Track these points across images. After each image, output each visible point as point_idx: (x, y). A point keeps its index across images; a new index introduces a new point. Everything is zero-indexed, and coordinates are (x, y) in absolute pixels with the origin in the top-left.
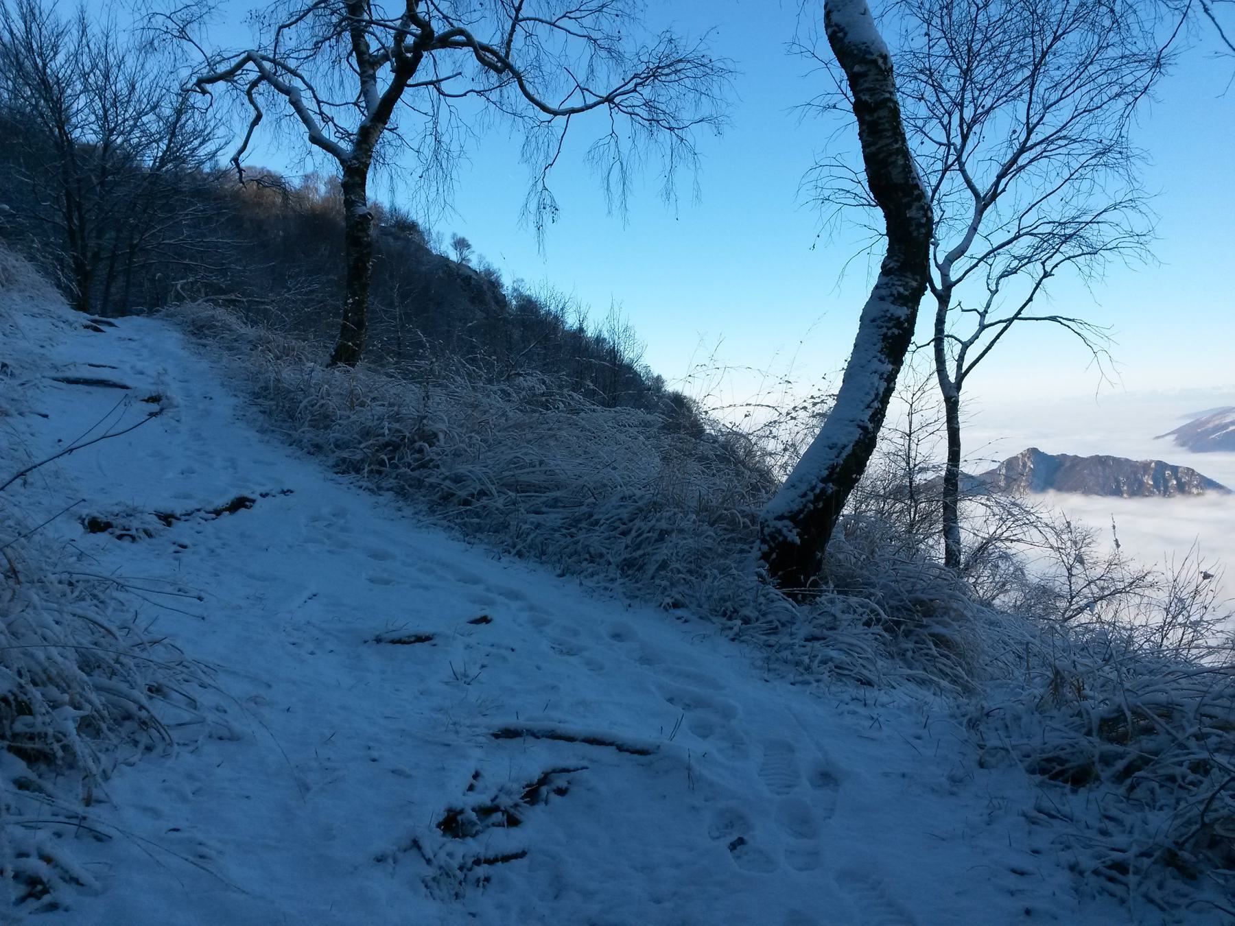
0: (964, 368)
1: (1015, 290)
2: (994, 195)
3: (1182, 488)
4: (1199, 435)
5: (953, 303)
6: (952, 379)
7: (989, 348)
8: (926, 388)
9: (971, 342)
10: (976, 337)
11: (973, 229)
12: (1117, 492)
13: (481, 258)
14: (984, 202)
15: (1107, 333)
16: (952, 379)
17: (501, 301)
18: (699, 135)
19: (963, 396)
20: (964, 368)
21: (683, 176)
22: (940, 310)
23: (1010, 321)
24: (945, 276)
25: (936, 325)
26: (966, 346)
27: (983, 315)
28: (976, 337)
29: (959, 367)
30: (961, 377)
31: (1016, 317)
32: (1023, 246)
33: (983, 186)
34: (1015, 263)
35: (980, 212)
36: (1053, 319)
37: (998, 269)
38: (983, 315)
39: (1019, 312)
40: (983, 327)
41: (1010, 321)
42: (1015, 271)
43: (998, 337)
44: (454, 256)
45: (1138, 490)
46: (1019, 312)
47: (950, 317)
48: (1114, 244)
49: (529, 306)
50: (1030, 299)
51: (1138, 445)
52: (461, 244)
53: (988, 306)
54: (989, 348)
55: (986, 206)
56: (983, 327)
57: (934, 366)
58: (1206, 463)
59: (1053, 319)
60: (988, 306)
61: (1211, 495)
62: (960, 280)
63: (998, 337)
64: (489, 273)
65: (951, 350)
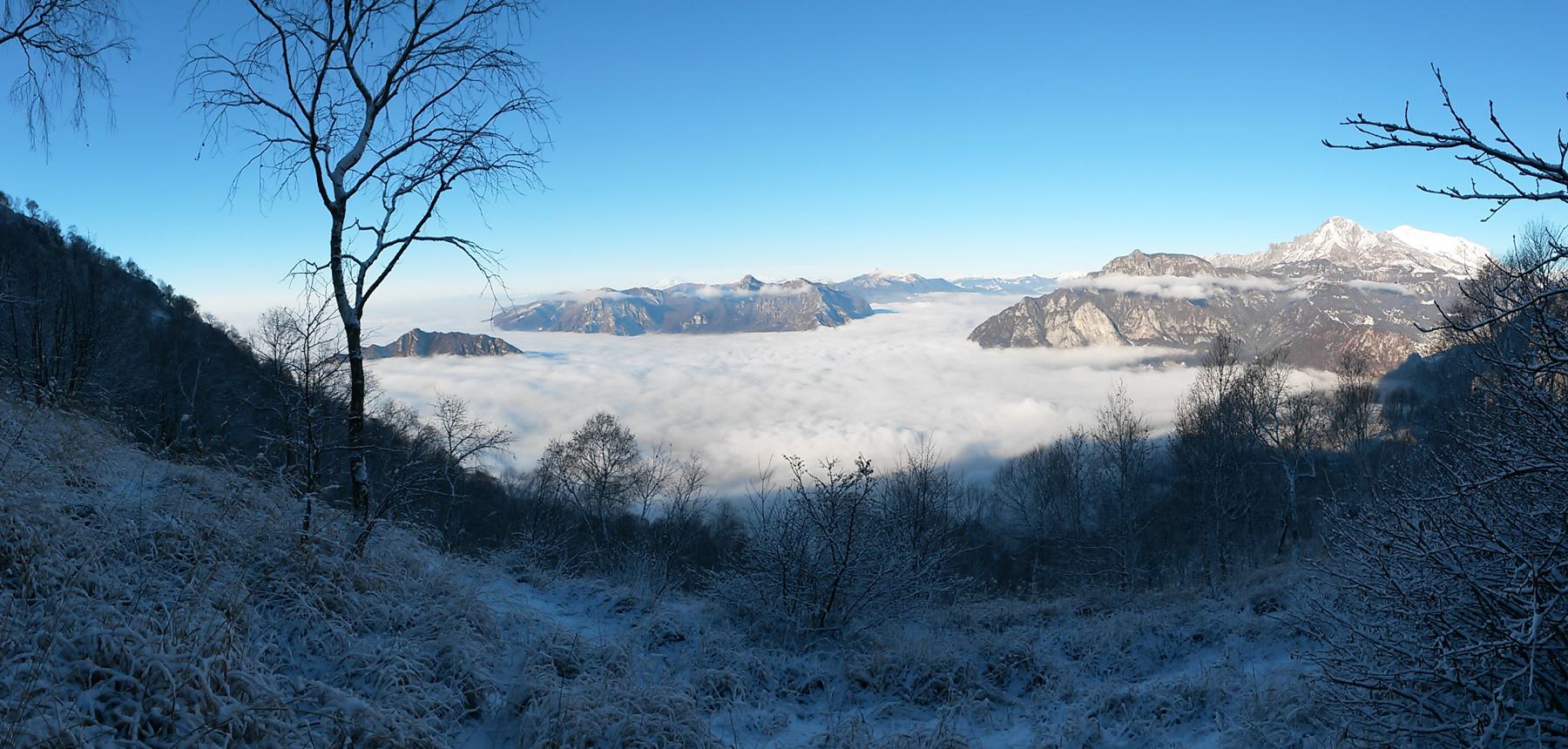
0: (364, 292)
1: (411, 208)
2: (385, 97)
3: (497, 351)
4: (507, 320)
5: (348, 221)
6: (352, 304)
7: (388, 270)
8: (323, 317)
9: (370, 263)
10: (374, 257)
11: (366, 134)
12: (463, 353)
13: (46, 214)
14: (375, 106)
15: (497, 257)
16: (352, 304)
17: (60, 241)
18: (109, 60)
19: (365, 323)
20: (364, 292)
21: (93, 99)
22: (335, 226)
23: (407, 241)
24: (338, 186)
25: (332, 243)
26: (364, 267)
27: (381, 234)
28: (374, 257)
29: (359, 290)
30: (361, 301)
31: (413, 237)
32: (419, 154)
33: (375, 91)
34: (408, 183)
35: (372, 116)
36: (449, 239)
37: (395, 184)
38: (381, 234)
39: (417, 230)
40: (381, 247)
41: (407, 241)
42: (409, 190)
43: (397, 257)
44: (28, 214)
45: (474, 352)
46: (417, 230)
47: (345, 236)
48: (504, 161)
49: (79, 243)
50: (428, 215)
51: (475, 325)
52: (32, 205)
53: (386, 224)
54: (388, 270)
55: (377, 109)
56: (381, 247)
57: (331, 289)
58: (510, 337)
59: (449, 239)
60: (386, 224)
61: (511, 355)
62: (353, 191)
63: (397, 257)
64: (51, 223)
65: (350, 272)
